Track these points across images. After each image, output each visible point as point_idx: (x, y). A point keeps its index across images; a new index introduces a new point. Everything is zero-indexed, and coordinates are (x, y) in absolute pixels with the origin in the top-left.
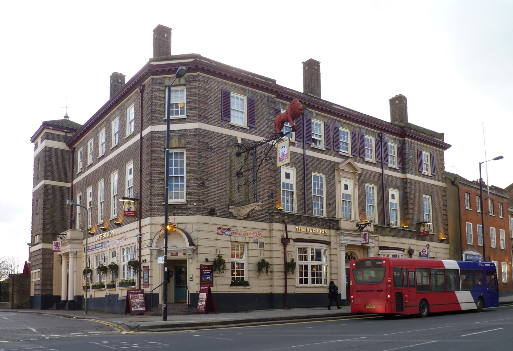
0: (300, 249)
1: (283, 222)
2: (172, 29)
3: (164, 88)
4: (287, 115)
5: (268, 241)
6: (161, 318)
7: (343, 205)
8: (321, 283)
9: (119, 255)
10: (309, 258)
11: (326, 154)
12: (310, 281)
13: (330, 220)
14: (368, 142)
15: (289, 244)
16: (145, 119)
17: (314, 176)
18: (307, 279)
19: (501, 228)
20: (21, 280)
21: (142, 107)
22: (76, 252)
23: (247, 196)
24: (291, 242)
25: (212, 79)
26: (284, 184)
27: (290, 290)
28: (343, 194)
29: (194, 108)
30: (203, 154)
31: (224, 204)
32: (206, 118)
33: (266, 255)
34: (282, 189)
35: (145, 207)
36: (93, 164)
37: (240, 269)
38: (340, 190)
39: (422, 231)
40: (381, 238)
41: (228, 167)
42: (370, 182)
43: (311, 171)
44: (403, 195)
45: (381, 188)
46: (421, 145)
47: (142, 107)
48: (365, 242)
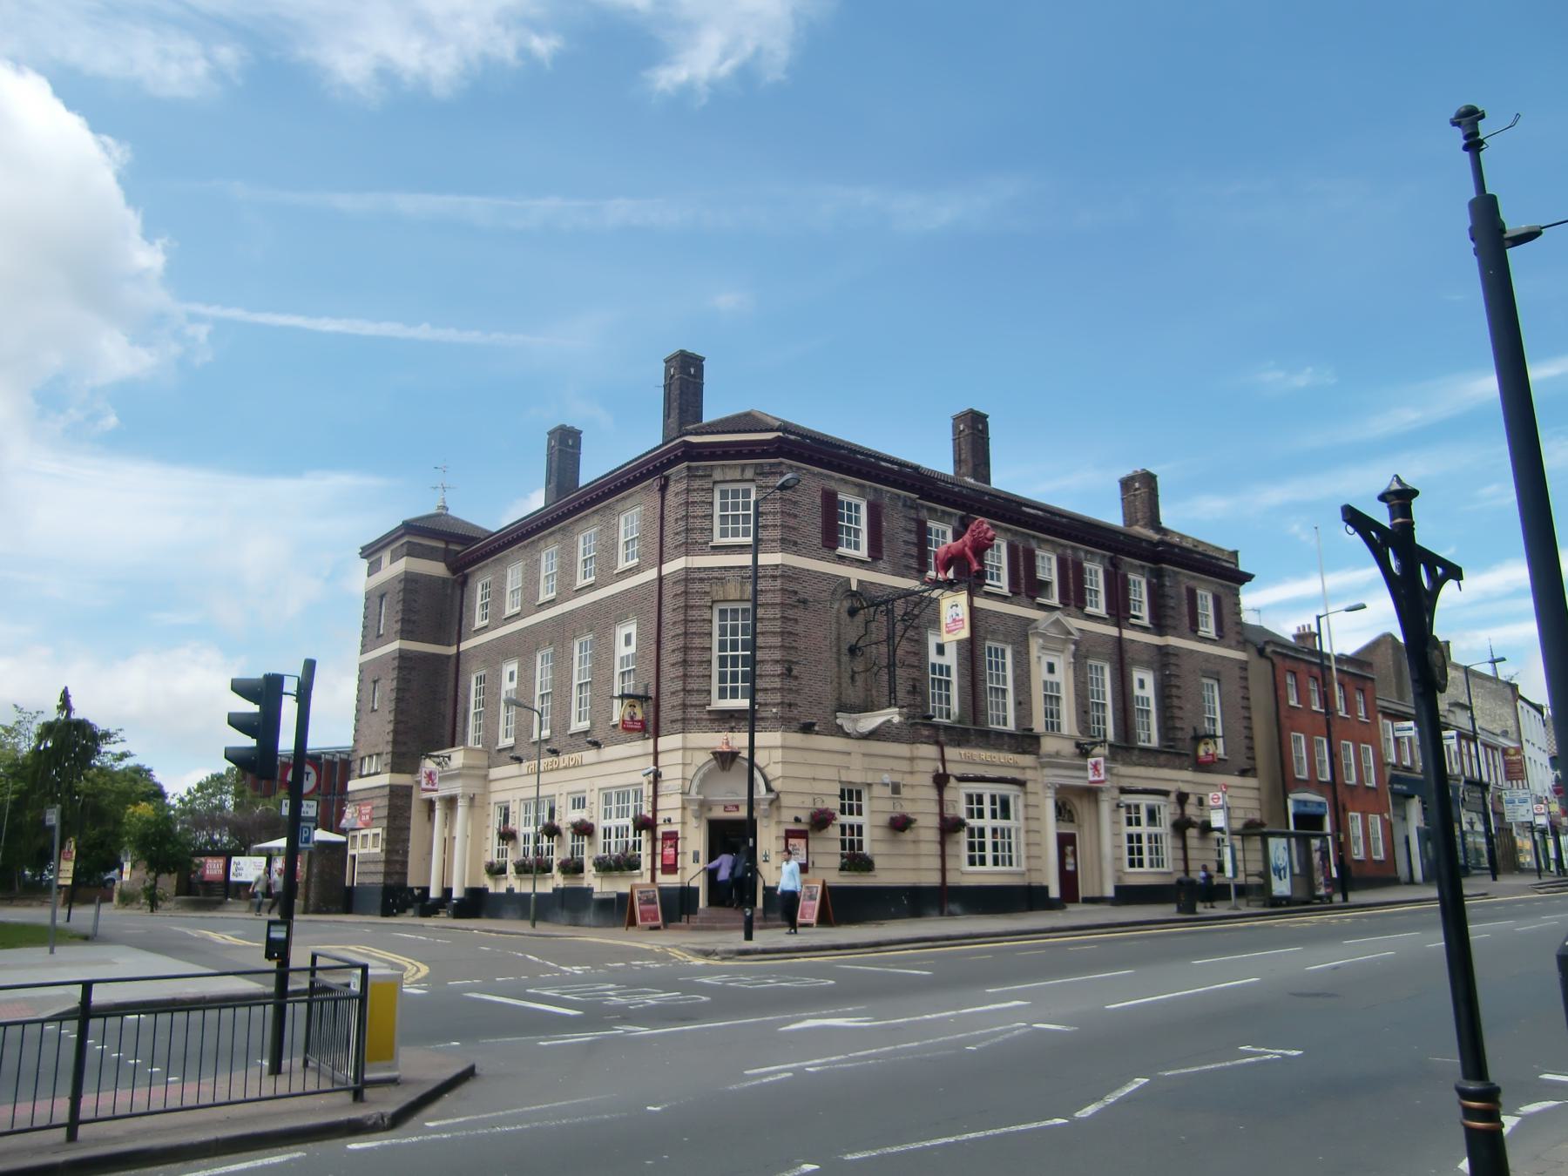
0: (970, 798)
1: (937, 743)
3: (711, 485)
6: (742, 934)
7: (1046, 704)
8: (1011, 864)
9: (595, 806)
10: (987, 813)
11: (1011, 603)
12: (989, 860)
13: (1023, 736)
14: (1091, 575)
16: (668, 541)
17: (990, 648)
19: (1365, 743)
20: (327, 851)
21: (662, 518)
22: (474, 795)
23: (869, 693)
24: (952, 781)
25: (805, 469)
26: (934, 665)
27: (953, 879)
28: (1045, 683)
29: (772, 525)
30: (790, 613)
31: (828, 710)
32: (795, 544)
33: (907, 809)
34: (931, 676)
35: (666, 713)
36: (523, 615)
38: (1039, 674)
39: (1201, 753)
41: (833, 637)
42: (1097, 656)
43: (985, 639)
44: (1162, 680)
45: (1118, 666)
47: (662, 518)
48: (1096, 778)
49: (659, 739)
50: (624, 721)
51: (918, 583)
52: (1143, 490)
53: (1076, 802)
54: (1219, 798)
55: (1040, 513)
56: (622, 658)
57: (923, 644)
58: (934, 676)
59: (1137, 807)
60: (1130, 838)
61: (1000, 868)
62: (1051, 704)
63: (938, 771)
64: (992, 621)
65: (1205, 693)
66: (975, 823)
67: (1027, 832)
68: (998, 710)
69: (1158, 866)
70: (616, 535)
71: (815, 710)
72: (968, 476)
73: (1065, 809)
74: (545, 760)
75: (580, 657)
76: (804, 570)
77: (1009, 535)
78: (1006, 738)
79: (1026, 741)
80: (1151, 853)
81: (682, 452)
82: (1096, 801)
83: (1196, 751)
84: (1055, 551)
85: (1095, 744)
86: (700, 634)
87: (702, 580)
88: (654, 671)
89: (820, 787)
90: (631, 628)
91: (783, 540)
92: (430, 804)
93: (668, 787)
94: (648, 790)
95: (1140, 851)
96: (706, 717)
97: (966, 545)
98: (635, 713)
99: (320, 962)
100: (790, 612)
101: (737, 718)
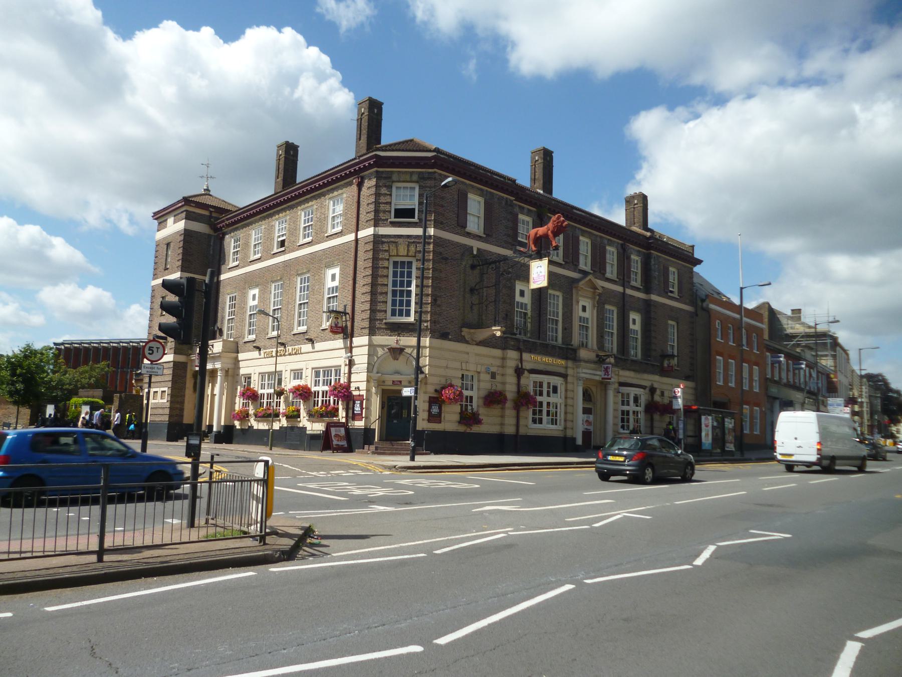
1: (518, 349)
2: (383, 103)
4: (548, 231)
5: (500, 371)
6: (408, 457)
7: (580, 330)
8: (556, 424)
11: (564, 268)
15: (524, 375)
17: (550, 294)
18: (542, 418)
22: (228, 369)
24: (526, 372)
26: (518, 303)
27: (522, 431)
28: (580, 317)
32: (442, 223)
34: (516, 309)
37: (464, 403)
39: (666, 365)
40: (622, 373)
42: (610, 303)
46: (668, 260)
48: (606, 377)
49: (353, 339)
50: (331, 327)
51: (512, 252)
52: (639, 205)
54: (679, 392)
55: (583, 214)
56: (329, 289)
57: (512, 289)
58: (518, 310)
59: (628, 395)
60: (623, 412)
68: (552, 332)
70: (327, 212)
72: (539, 189)
74: (280, 349)
75: (301, 288)
79: (569, 352)
81: (374, 161)
83: (662, 364)
85: (608, 356)
88: (350, 297)
89: (450, 373)
90: (336, 271)
93: (358, 368)
94: (344, 370)
96: (384, 326)
97: (549, 230)
98: (338, 323)
99: (216, 459)
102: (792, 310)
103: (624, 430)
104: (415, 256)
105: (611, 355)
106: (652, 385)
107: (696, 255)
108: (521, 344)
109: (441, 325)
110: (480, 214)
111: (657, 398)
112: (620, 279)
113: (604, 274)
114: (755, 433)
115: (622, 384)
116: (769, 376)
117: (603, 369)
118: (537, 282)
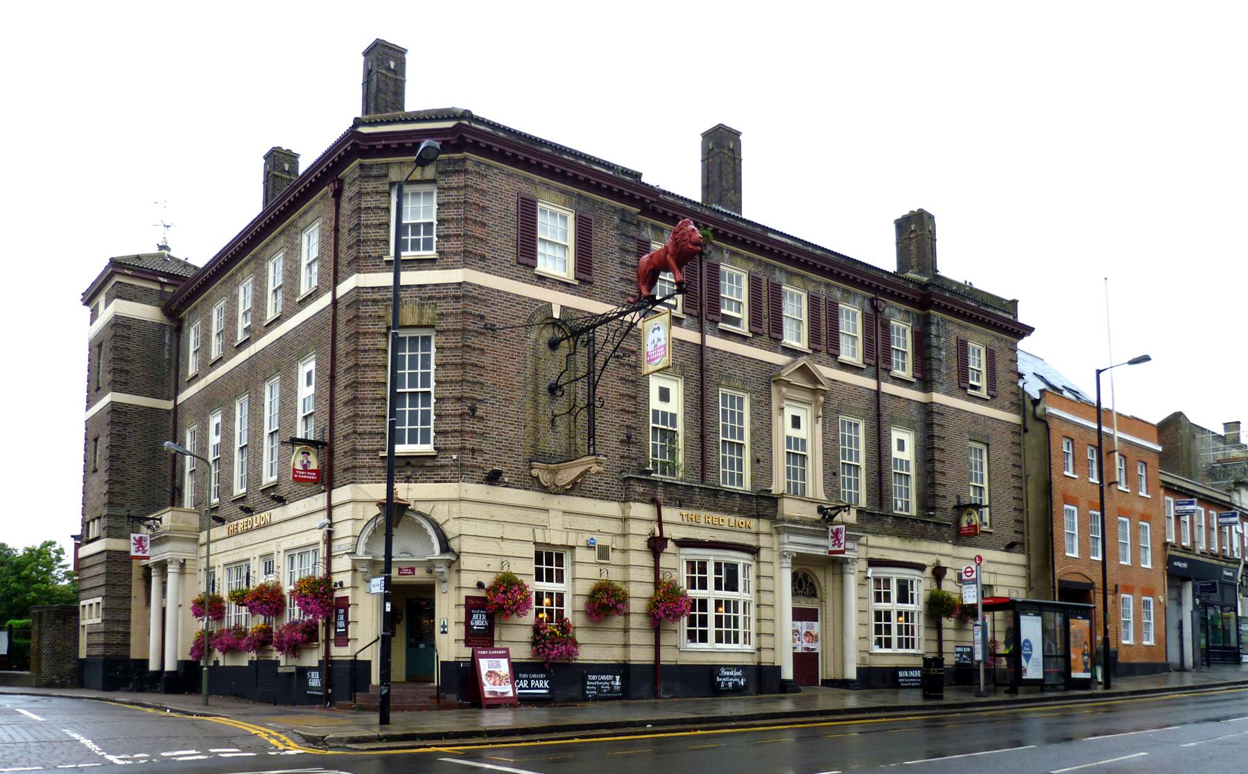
0: (691, 564)
1: (654, 501)
3: (387, 188)
5: (618, 543)
7: (788, 462)
11: (752, 345)
24: (670, 544)
26: (655, 412)
27: (668, 657)
28: (789, 438)
29: (455, 235)
31: (521, 459)
32: (483, 258)
34: (652, 425)
35: (340, 462)
38: (783, 428)
39: (964, 525)
40: (873, 540)
41: (529, 372)
45: (874, 424)
48: (836, 548)
49: (333, 492)
53: (820, 575)
54: (972, 571)
55: (789, 242)
60: (878, 615)
61: (723, 646)
62: (795, 463)
63: (654, 534)
64: (728, 364)
65: (972, 458)
66: (697, 594)
67: (758, 606)
68: (850, 487)
69: (907, 647)
71: (505, 458)
73: (807, 582)
76: (493, 290)
77: (752, 265)
78: (738, 500)
80: (900, 633)
82: (842, 574)
83: (958, 521)
84: (805, 288)
85: (839, 509)
86: (373, 366)
87: (375, 301)
89: (508, 548)
91: (466, 253)
92: (147, 569)
94: (322, 549)
95: (888, 628)
100: (475, 340)
101: (413, 466)
102: (1226, 425)
103: (881, 647)
104: (432, 327)
105: (843, 507)
106: (938, 562)
107: (1022, 319)
108: (660, 490)
109: (487, 457)
110: (566, 241)
111: (949, 586)
112: (869, 365)
113: (836, 356)
114: (1145, 643)
115: (873, 563)
116: (1171, 539)
117: (830, 534)
118: (654, 359)
